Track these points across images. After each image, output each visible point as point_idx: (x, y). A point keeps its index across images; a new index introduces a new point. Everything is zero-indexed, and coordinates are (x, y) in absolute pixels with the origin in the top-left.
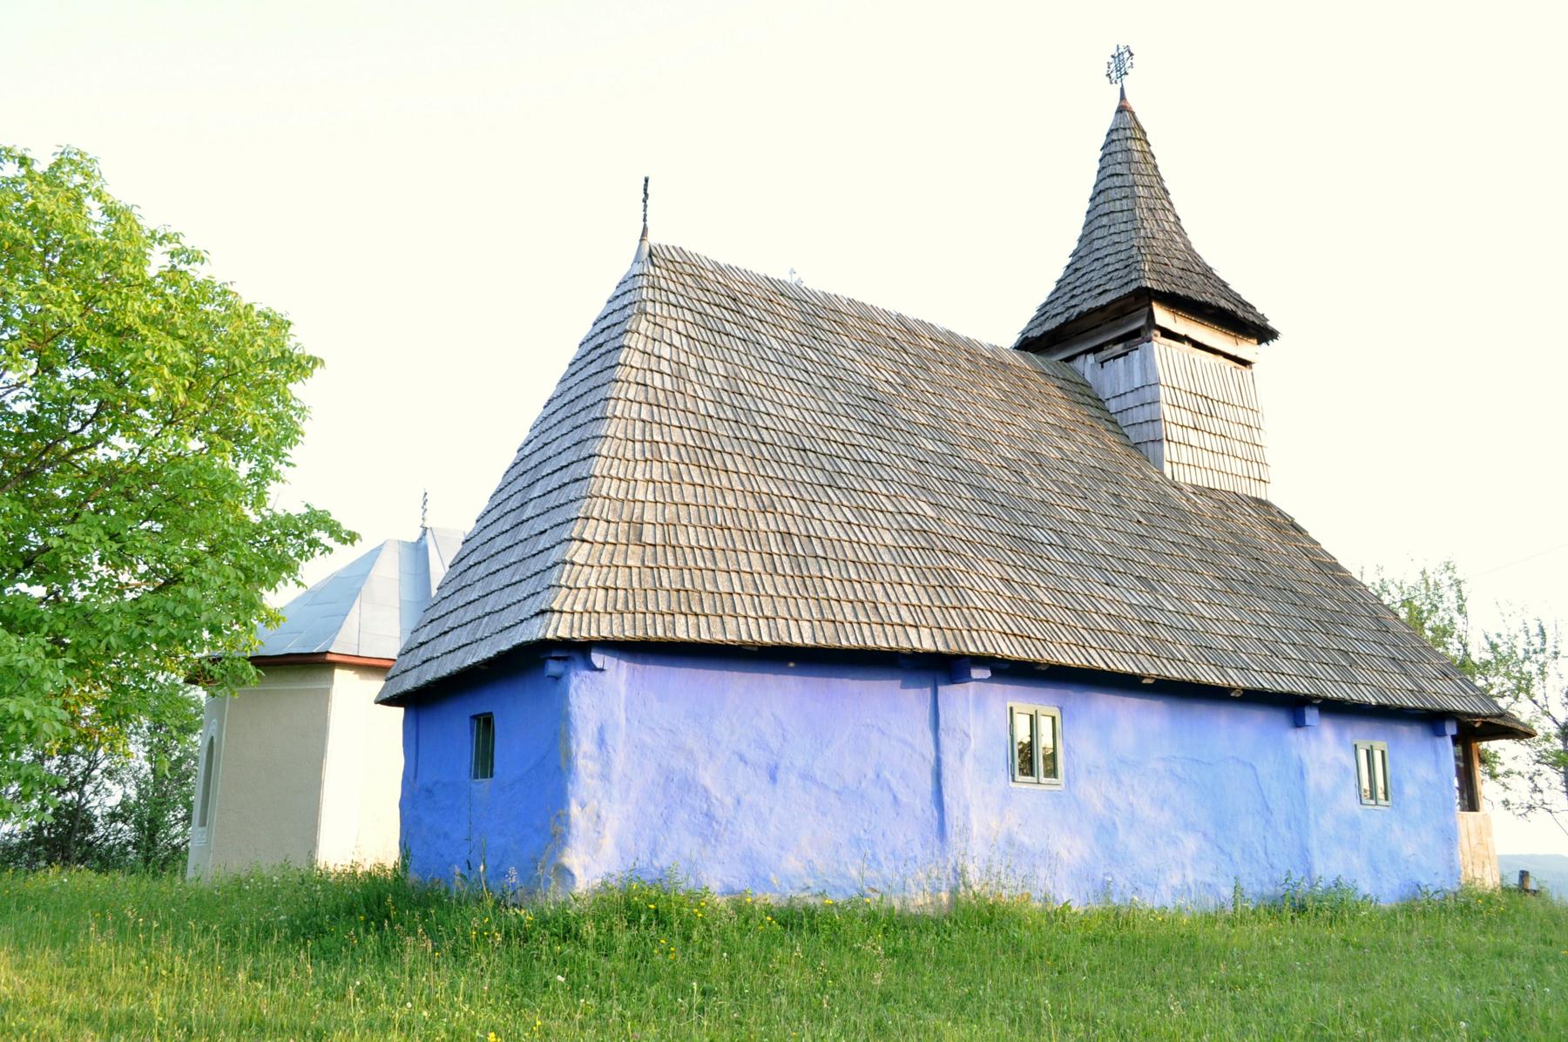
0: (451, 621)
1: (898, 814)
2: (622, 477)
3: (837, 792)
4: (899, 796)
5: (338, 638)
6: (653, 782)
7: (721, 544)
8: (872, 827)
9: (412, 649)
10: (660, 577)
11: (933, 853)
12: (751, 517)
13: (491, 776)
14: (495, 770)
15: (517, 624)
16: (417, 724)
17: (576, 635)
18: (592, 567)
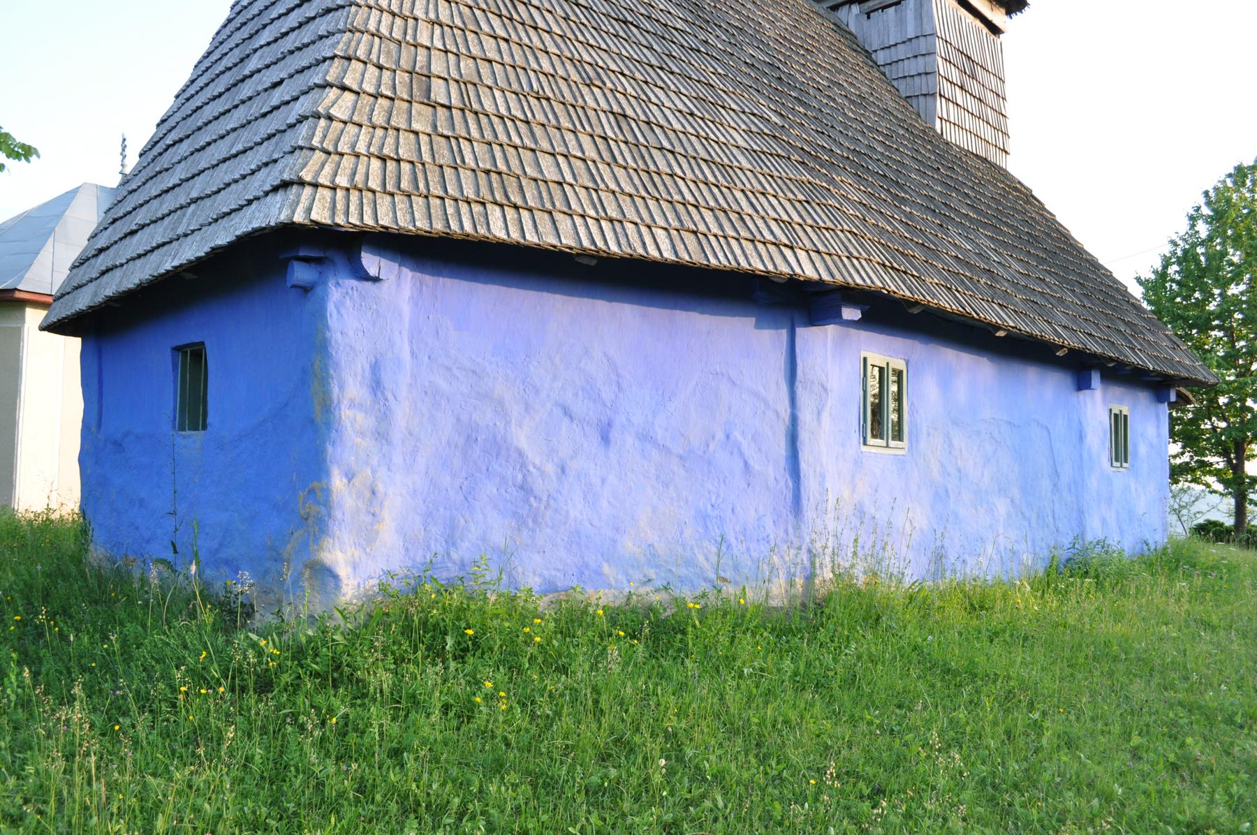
0: (140, 217)
1: (749, 485)
2: (396, 11)
3: (681, 457)
4: (751, 462)
5: (27, 276)
6: (448, 443)
7: (540, 117)
8: (720, 501)
9: (88, 259)
10: (460, 151)
11: (786, 532)
12: (574, 88)
13: (204, 427)
14: (209, 420)
15: (241, 207)
16: (100, 358)
17: (340, 220)
18: (361, 126)
